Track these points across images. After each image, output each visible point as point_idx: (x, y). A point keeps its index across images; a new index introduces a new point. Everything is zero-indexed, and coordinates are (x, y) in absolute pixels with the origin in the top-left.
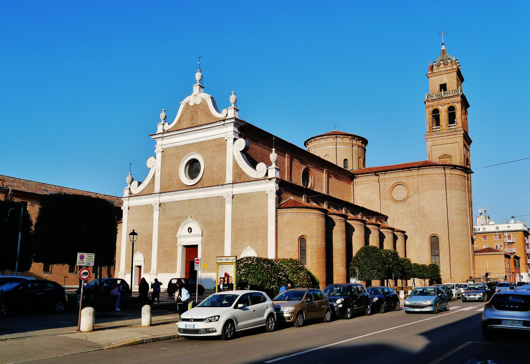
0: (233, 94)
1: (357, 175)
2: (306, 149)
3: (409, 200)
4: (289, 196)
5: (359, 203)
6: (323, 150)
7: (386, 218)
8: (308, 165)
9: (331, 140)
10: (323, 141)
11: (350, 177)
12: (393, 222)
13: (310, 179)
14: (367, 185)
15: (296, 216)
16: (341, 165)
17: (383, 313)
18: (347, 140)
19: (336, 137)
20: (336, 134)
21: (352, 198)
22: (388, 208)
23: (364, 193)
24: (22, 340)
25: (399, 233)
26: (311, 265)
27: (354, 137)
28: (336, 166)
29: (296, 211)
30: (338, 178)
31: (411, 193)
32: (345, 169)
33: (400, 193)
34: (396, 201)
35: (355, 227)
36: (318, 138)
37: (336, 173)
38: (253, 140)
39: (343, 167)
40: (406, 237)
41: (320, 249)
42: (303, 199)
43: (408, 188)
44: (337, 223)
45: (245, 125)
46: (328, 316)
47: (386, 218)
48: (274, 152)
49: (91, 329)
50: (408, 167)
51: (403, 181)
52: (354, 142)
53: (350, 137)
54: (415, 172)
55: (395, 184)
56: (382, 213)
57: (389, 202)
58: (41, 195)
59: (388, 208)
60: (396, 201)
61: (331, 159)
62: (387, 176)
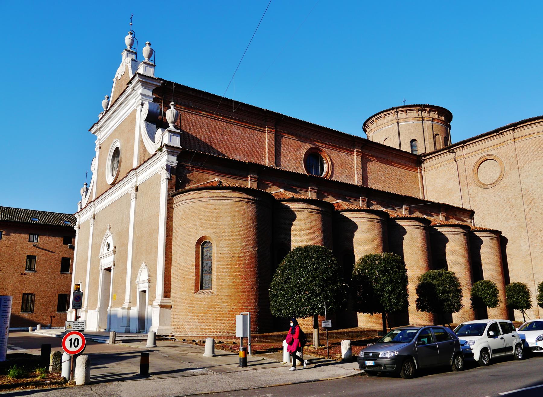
0: (147, 45)
1: (425, 156)
2: (363, 136)
3: (505, 180)
4: (211, 177)
5: (431, 197)
6: (382, 133)
7: (471, 214)
8: (318, 144)
9: (391, 117)
10: (380, 121)
11: (414, 161)
12: (483, 219)
13: (325, 165)
14: (440, 169)
15: (188, 205)
16: (406, 148)
17: (408, 377)
18: (413, 114)
19: (397, 112)
20: (397, 109)
21: (421, 191)
22: (474, 197)
23: (438, 182)
24: (219, 376)
25: (485, 234)
26: (218, 290)
27: (423, 108)
28: (400, 151)
29: (194, 196)
30: (382, 161)
31: (507, 168)
32: (414, 153)
33: (489, 172)
34: (485, 186)
35: (357, 223)
36: (374, 119)
37: (383, 156)
38: (188, 107)
39: (410, 151)
40: (502, 242)
41: (240, 258)
42: (361, 202)
43: (501, 163)
44: (300, 215)
45: (164, 83)
46: (460, 363)
47: (471, 214)
48: (172, 107)
49: (83, 383)
50: (498, 131)
51: (492, 153)
52: (425, 114)
53: (417, 108)
54: (508, 135)
55: (481, 160)
56: (465, 207)
57: (473, 189)
58: (19, 222)
59: (474, 197)
60: (485, 186)
61: (393, 143)
62: (467, 150)
